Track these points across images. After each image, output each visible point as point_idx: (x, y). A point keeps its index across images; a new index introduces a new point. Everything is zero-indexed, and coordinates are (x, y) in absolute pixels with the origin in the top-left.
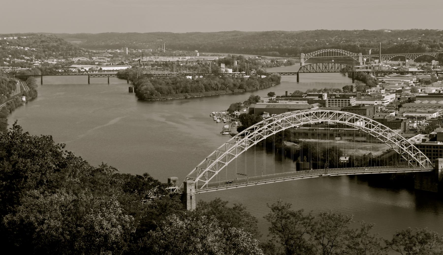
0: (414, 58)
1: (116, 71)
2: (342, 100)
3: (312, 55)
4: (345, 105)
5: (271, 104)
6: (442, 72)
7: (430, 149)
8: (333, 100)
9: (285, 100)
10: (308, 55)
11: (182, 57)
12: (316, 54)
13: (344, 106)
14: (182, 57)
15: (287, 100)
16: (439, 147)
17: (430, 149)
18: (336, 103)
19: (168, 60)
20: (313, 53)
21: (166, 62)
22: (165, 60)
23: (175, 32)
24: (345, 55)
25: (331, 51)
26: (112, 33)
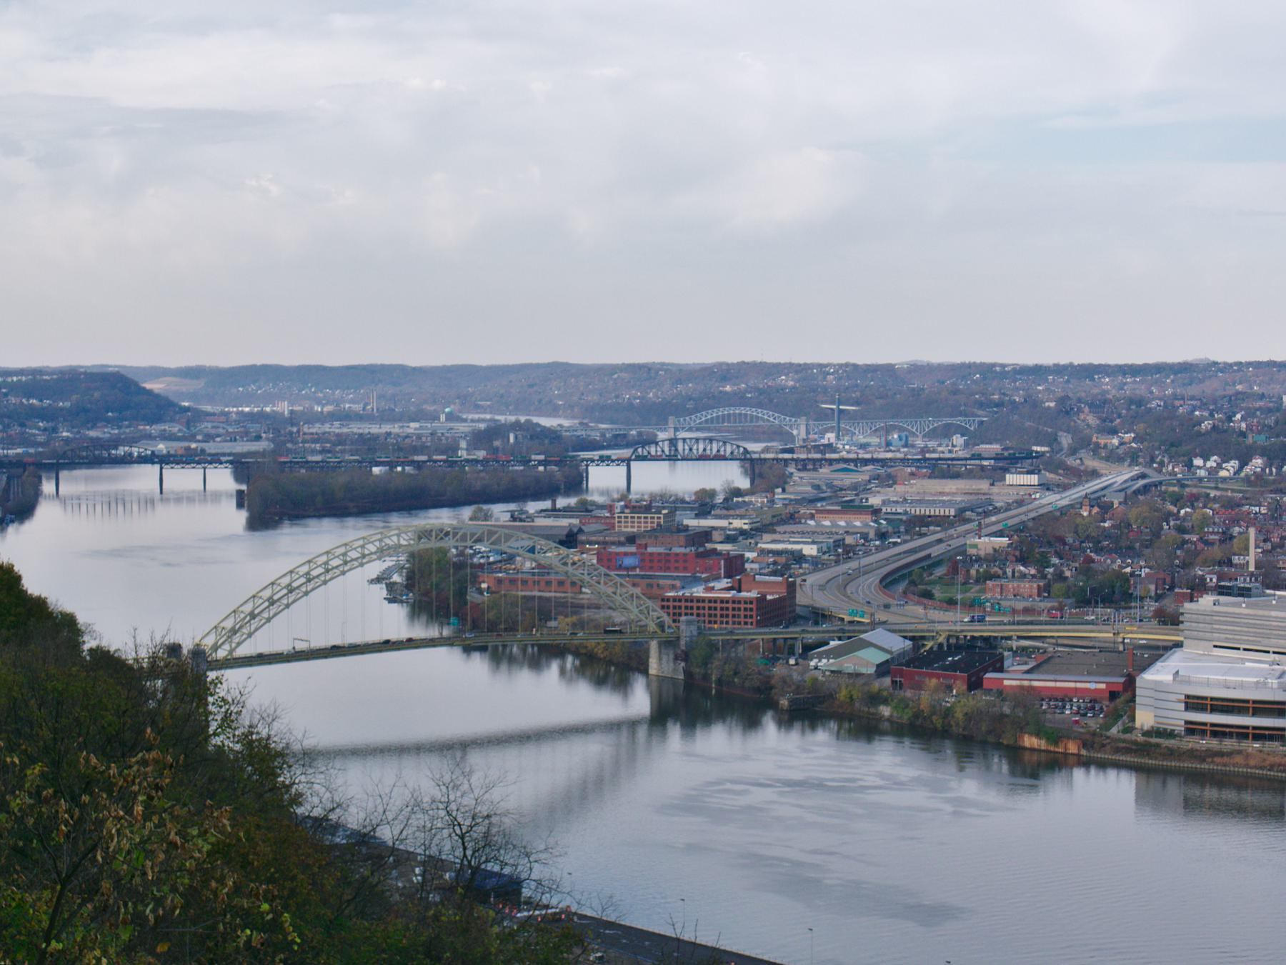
0: (924, 430)
1: (1173, 641)
2: (639, 518)
3: (695, 421)
4: (645, 527)
5: (681, 572)
6: (1282, 485)
7: (710, 612)
8: (626, 517)
9: (545, 517)
10: (685, 420)
11: (401, 425)
12: (703, 419)
13: (643, 529)
14: (401, 425)
15: (549, 517)
16: (695, 601)
17: (710, 612)
18: (633, 522)
19: (367, 431)
20: (696, 417)
21: (361, 435)
22: (361, 431)
23: (1141, 363)
24: (768, 421)
25: (737, 412)
26: (962, 363)
